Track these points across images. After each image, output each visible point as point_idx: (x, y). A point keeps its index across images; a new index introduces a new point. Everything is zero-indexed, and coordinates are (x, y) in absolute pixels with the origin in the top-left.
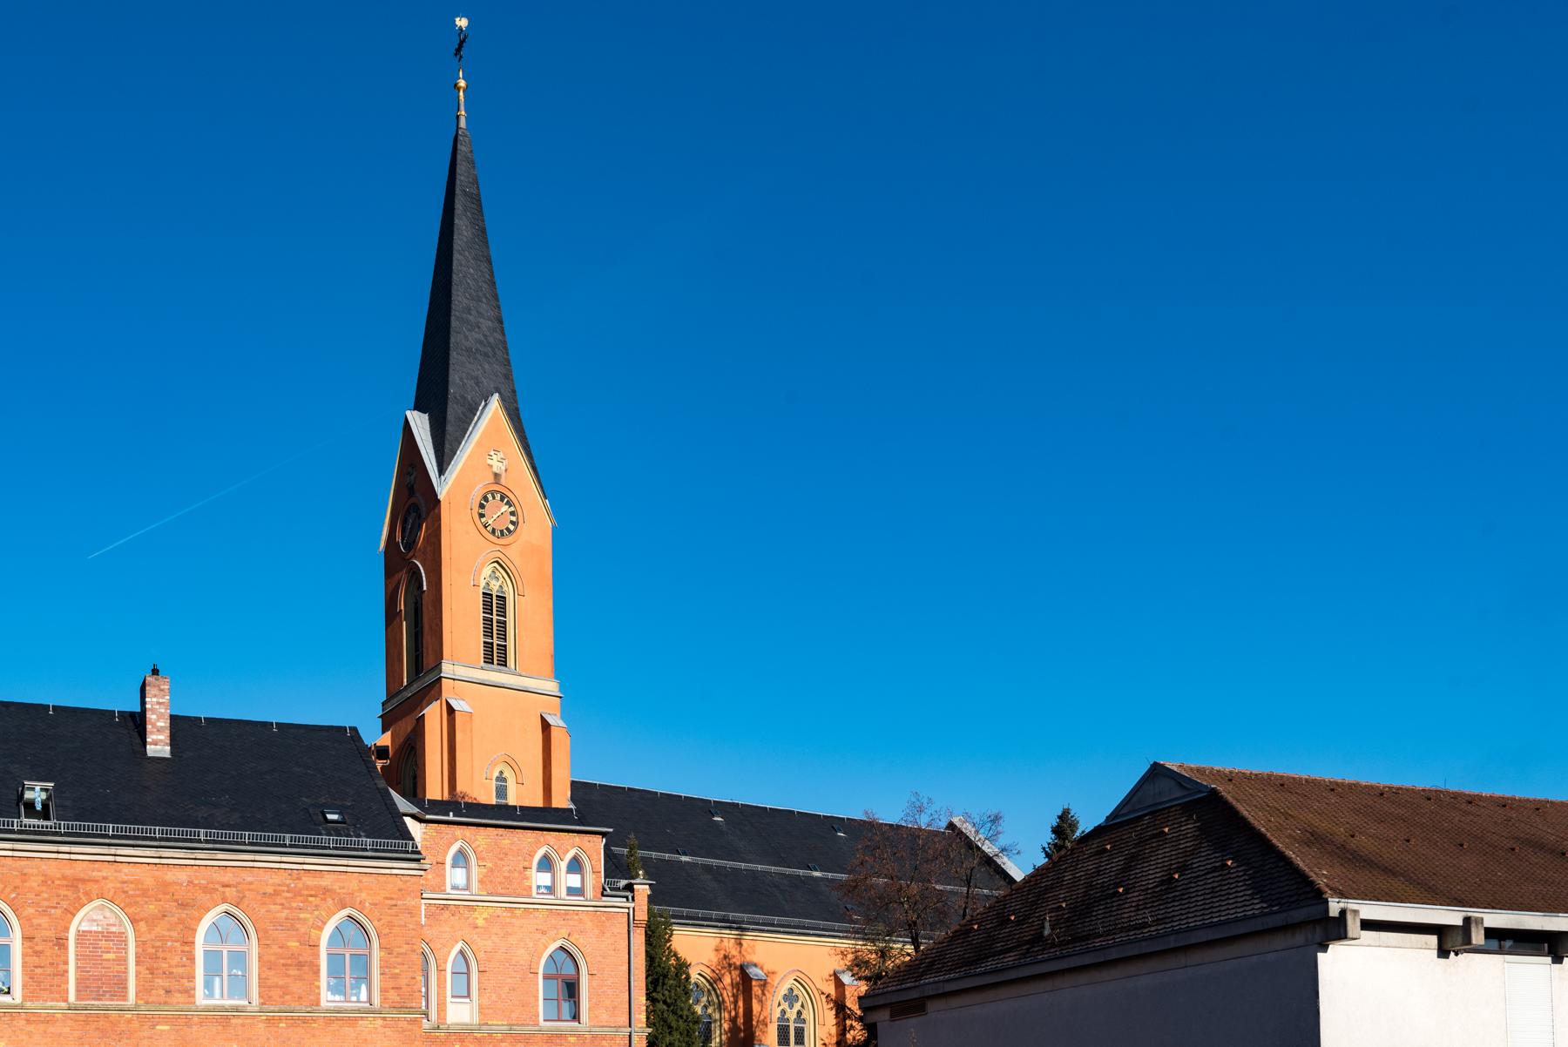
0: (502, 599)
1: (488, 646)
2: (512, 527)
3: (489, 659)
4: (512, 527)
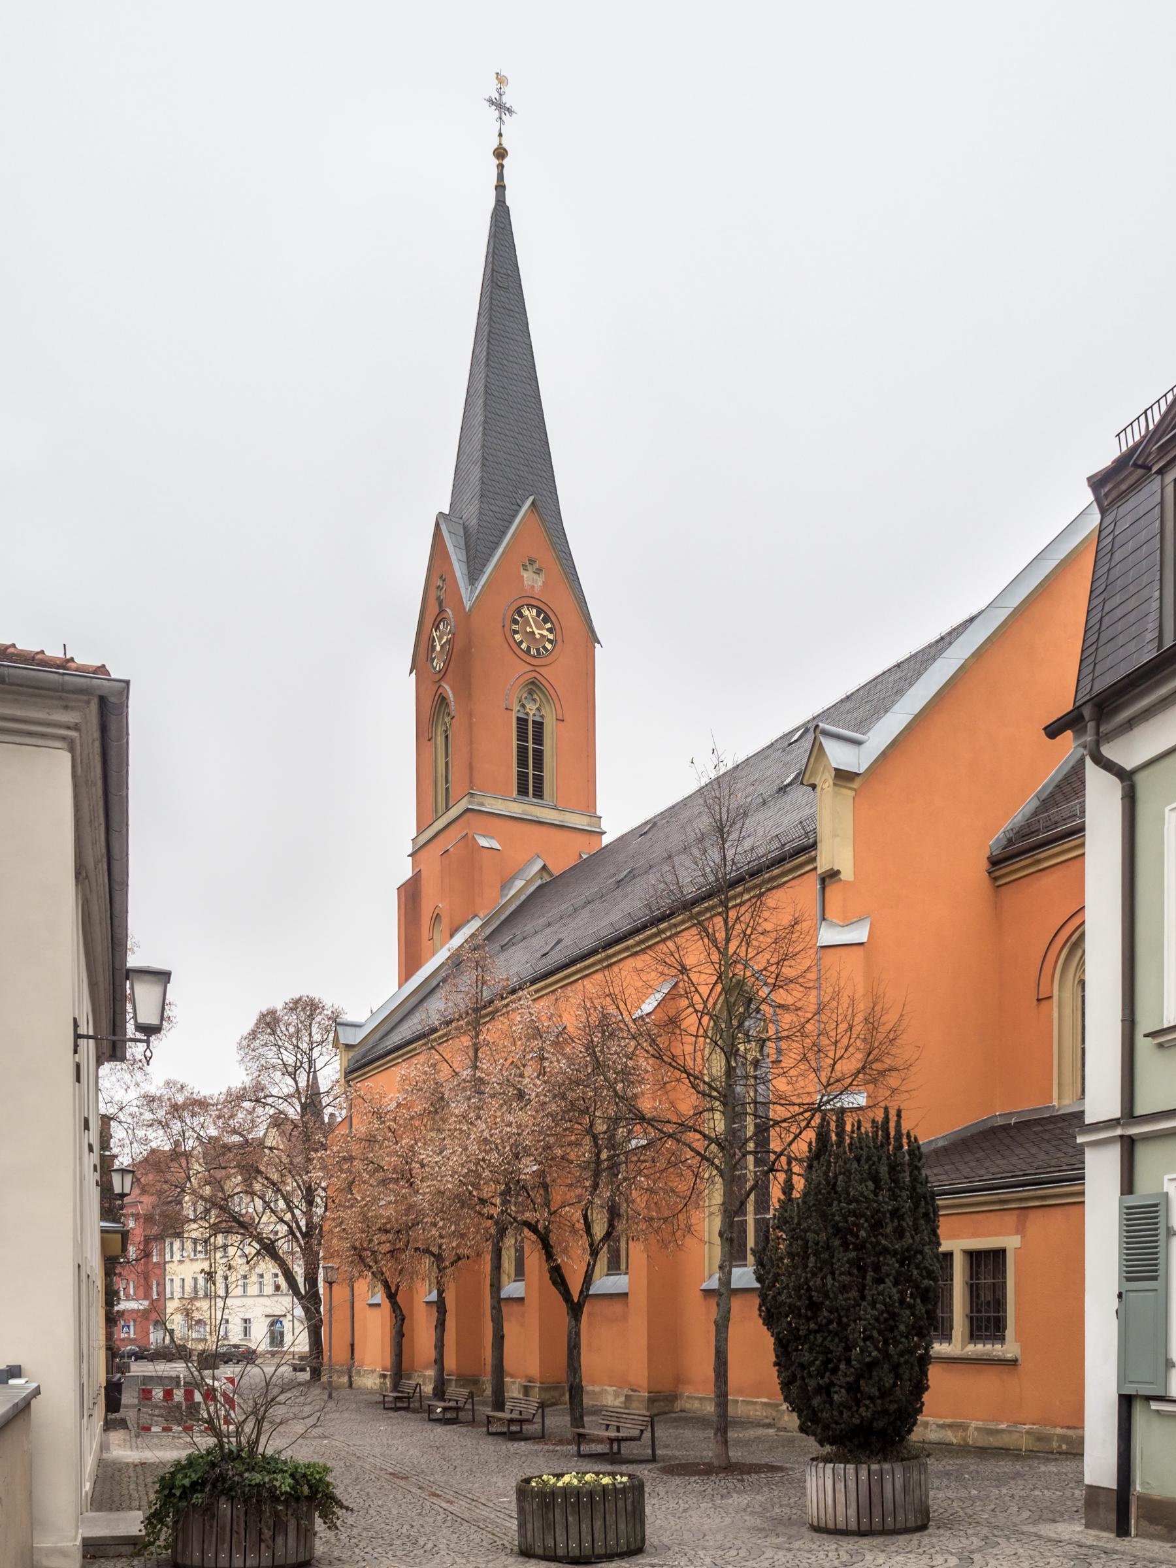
0: (539, 726)
1: (522, 778)
2: (549, 646)
3: (522, 790)
4: (549, 646)
